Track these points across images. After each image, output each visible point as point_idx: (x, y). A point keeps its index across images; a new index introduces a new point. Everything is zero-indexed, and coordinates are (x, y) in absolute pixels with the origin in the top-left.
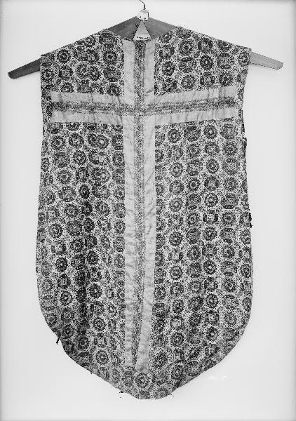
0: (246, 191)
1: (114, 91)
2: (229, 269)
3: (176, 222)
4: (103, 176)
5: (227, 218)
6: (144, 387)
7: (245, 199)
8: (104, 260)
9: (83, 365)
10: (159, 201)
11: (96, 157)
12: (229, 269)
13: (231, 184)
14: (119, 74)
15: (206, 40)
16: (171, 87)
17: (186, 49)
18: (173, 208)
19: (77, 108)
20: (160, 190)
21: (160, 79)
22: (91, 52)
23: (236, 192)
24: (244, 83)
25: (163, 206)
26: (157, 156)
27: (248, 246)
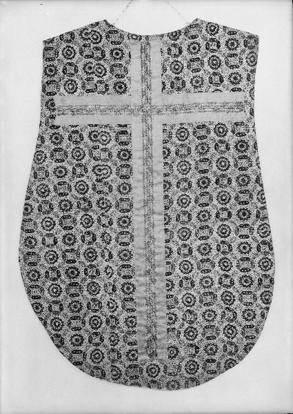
0: (261, 185)
1: (121, 88)
2: (245, 265)
3: (185, 218)
4: (105, 172)
5: (126, 189)
6: (99, 363)
7: (261, 193)
8: (103, 256)
9: (76, 364)
10: (166, 197)
11: (95, 153)
12: (245, 265)
13: (243, 181)
14: (126, 70)
15: (251, 37)
16: (177, 85)
17: (231, 44)
18: (181, 202)
19: (202, 109)
20: (167, 185)
21: (169, 77)
22: (97, 49)
23: (250, 187)
24: (253, 82)
25: (171, 202)
26: (164, 153)
27: (267, 239)
